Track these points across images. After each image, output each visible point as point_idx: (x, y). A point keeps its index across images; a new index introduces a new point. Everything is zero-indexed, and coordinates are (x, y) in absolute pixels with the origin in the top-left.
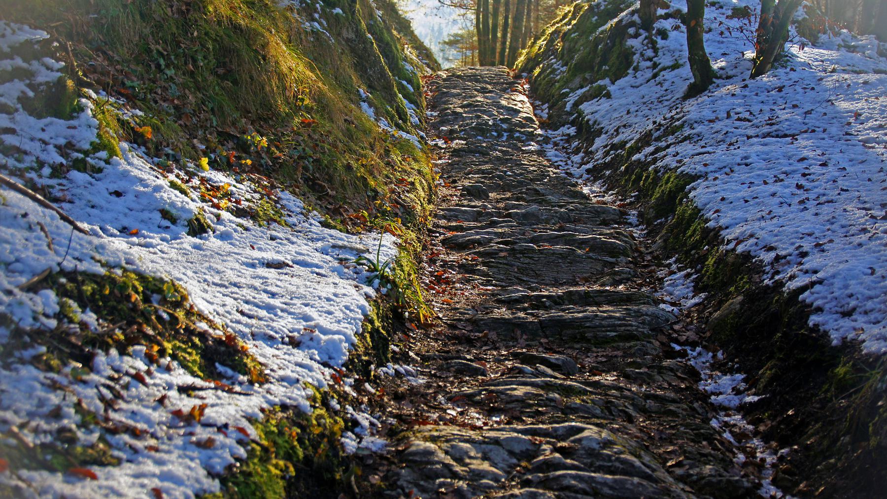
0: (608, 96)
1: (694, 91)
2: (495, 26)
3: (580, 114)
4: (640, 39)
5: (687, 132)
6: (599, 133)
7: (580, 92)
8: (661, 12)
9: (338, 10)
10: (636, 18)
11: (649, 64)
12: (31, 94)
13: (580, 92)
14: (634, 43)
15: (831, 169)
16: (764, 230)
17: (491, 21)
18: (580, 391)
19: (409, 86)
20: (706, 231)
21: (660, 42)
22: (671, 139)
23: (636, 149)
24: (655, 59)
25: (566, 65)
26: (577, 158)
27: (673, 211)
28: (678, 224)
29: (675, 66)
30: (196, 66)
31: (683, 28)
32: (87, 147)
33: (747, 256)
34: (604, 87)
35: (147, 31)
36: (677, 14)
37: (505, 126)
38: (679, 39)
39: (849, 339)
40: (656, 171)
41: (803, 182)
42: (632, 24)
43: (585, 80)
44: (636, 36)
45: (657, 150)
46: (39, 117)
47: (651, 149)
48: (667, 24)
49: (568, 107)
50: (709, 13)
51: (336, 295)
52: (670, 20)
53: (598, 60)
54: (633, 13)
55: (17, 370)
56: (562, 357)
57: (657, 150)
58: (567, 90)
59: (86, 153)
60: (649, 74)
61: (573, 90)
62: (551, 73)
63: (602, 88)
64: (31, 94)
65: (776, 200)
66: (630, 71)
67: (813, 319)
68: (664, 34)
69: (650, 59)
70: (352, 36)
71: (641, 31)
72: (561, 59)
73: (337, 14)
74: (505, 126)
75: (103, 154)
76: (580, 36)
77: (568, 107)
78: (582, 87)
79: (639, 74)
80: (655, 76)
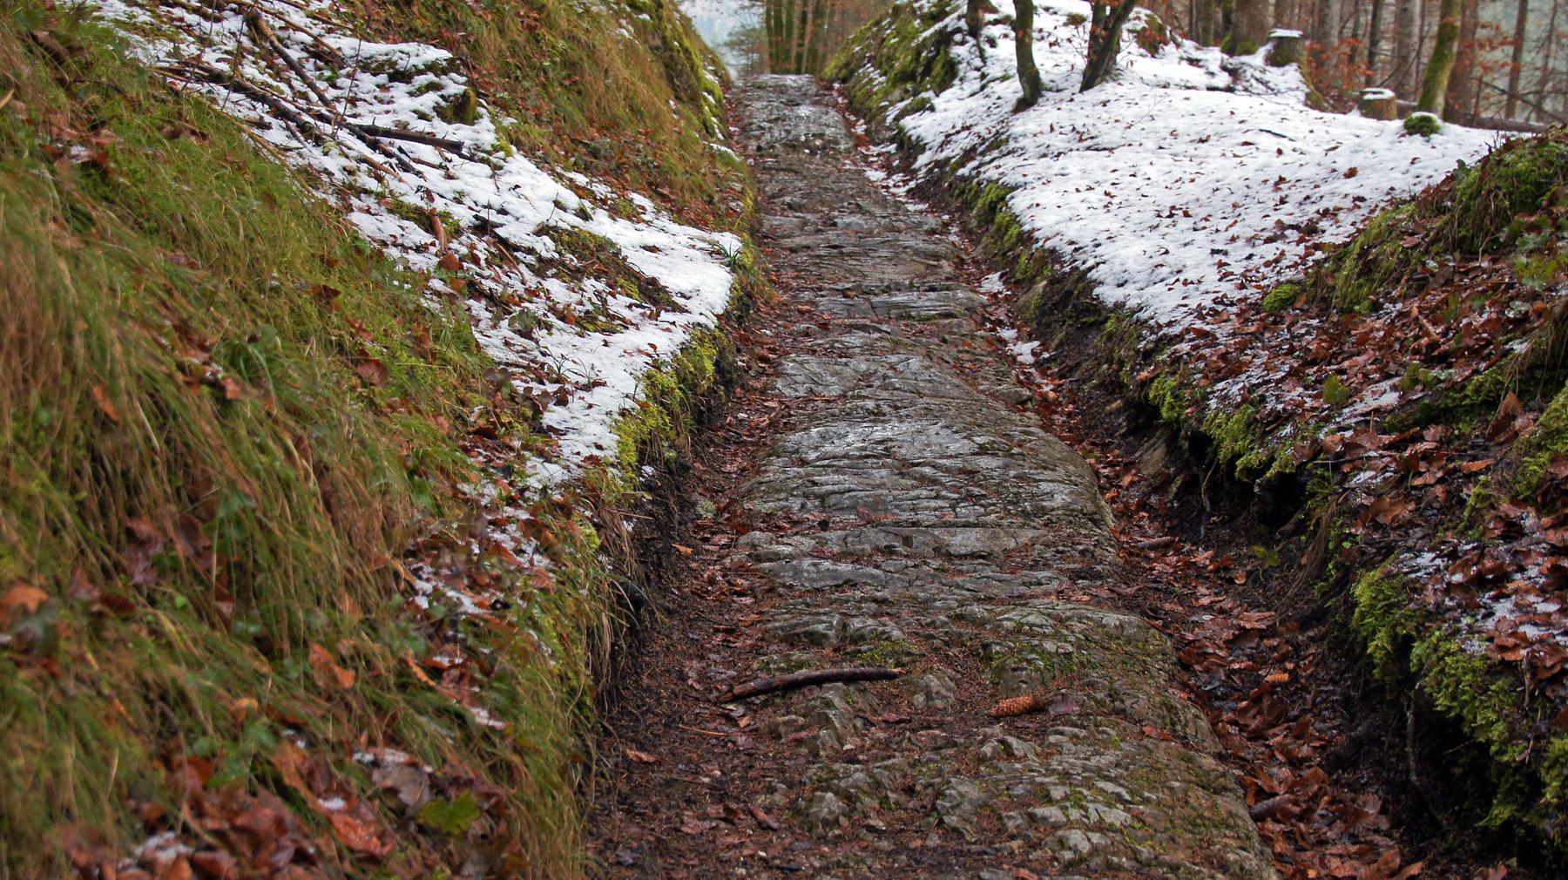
0: (932, 109)
1: (1023, 105)
2: (790, 23)
3: (901, 130)
4: (967, 46)
5: (1012, 145)
6: (923, 149)
7: (901, 105)
8: (990, 17)
9: (645, 16)
11: (977, 74)
12: (443, 104)
13: (901, 105)
14: (958, 51)
15: (1139, 182)
16: (1072, 231)
17: (784, 16)
20: (1021, 234)
21: (989, 51)
22: (995, 153)
23: (962, 164)
25: (885, 74)
26: (898, 177)
27: (992, 220)
28: (998, 230)
29: (1004, 78)
30: (547, 79)
31: (1013, 34)
32: (489, 148)
33: (1053, 251)
34: (929, 100)
35: (504, 46)
36: (1005, 20)
37: (818, 142)
38: (1006, 50)
40: (979, 184)
41: (1111, 190)
42: (959, 30)
43: (907, 91)
44: (963, 43)
45: (981, 165)
46: (449, 123)
47: (974, 164)
48: (995, 31)
49: (889, 120)
50: (1040, 21)
51: (318, 601)
52: (1000, 26)
53: (920, 70)
54: (959, 18)
55: (136, 480)
57: (981, 165)
59: (489, 153)
60: (977, 85)
61: (892, 104)
63: (925, 101)
64: (443, 104)
65: (1085, 205)
66: (956, 82)
67: (1097, 291)
68: (992, 42)
69: (978, 69)
70: (658, 42)
73: (644, 21)
74: (818, 142)
75: (501, 154)
76: (901, 41)
77: (889, 120)
78: (902, 100)
79: (965, 85)
80: (983, 88)
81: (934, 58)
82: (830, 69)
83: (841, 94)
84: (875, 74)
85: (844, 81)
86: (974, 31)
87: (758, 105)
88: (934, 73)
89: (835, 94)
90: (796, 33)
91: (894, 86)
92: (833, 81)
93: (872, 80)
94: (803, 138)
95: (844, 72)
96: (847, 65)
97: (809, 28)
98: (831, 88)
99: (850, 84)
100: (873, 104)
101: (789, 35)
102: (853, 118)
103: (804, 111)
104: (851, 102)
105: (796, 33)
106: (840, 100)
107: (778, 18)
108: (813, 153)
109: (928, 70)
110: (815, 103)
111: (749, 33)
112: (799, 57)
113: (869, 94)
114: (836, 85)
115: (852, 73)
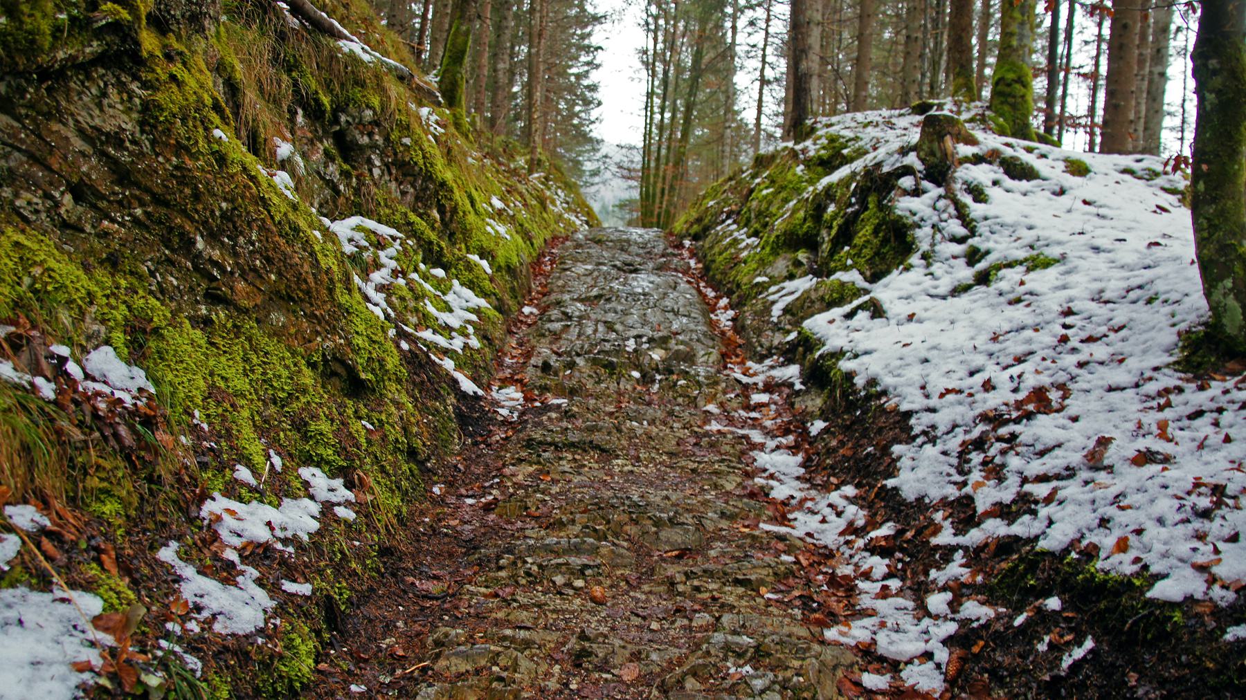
2: (654, 195)
8: (964, 150)
10: (912, 159)
18: (1230, 137)
19: (484, 263)
24: (970, 241)
25: (756, 234)
39: (1160, 591)
43: (798, 264)
44: (917, 192)
52: (984, 166)
56: (1025, 615)
58: (765, 279)
62: (730, 245)
66: (915, 259)
71: (926, 184)
72: (746, 225)
74: (657, 355)
81: (856, 214)
82: (679, 225)
83: (693, 254)
84: (741, 234)
85: (696, 238)
86: (939, 172)
87: (581, 269)
88: (857, 241)
89: (686, 254)
90: (657, 201)
91: (775, 252)
92: (683, 237)
93: (736, 241)
94: (631, 345)
95: (696, 228)
96: (699, 220)
97: (666, 197)
98: (680, 246)
99: (707, 243)
100: (743, 275)
101: (654, 202)
102: (711, 293)
103: (642, 282)
104: (707, 269)
105: (657, 201)
106: (692, 263)
107: (647, 191)
108: (646, 379)
109: (845, 235)
110: (660, 268)
111: (631, 201)
112: (659, 215)
113: (735, 262)
114: (687, 243)
115: (706, 229)
